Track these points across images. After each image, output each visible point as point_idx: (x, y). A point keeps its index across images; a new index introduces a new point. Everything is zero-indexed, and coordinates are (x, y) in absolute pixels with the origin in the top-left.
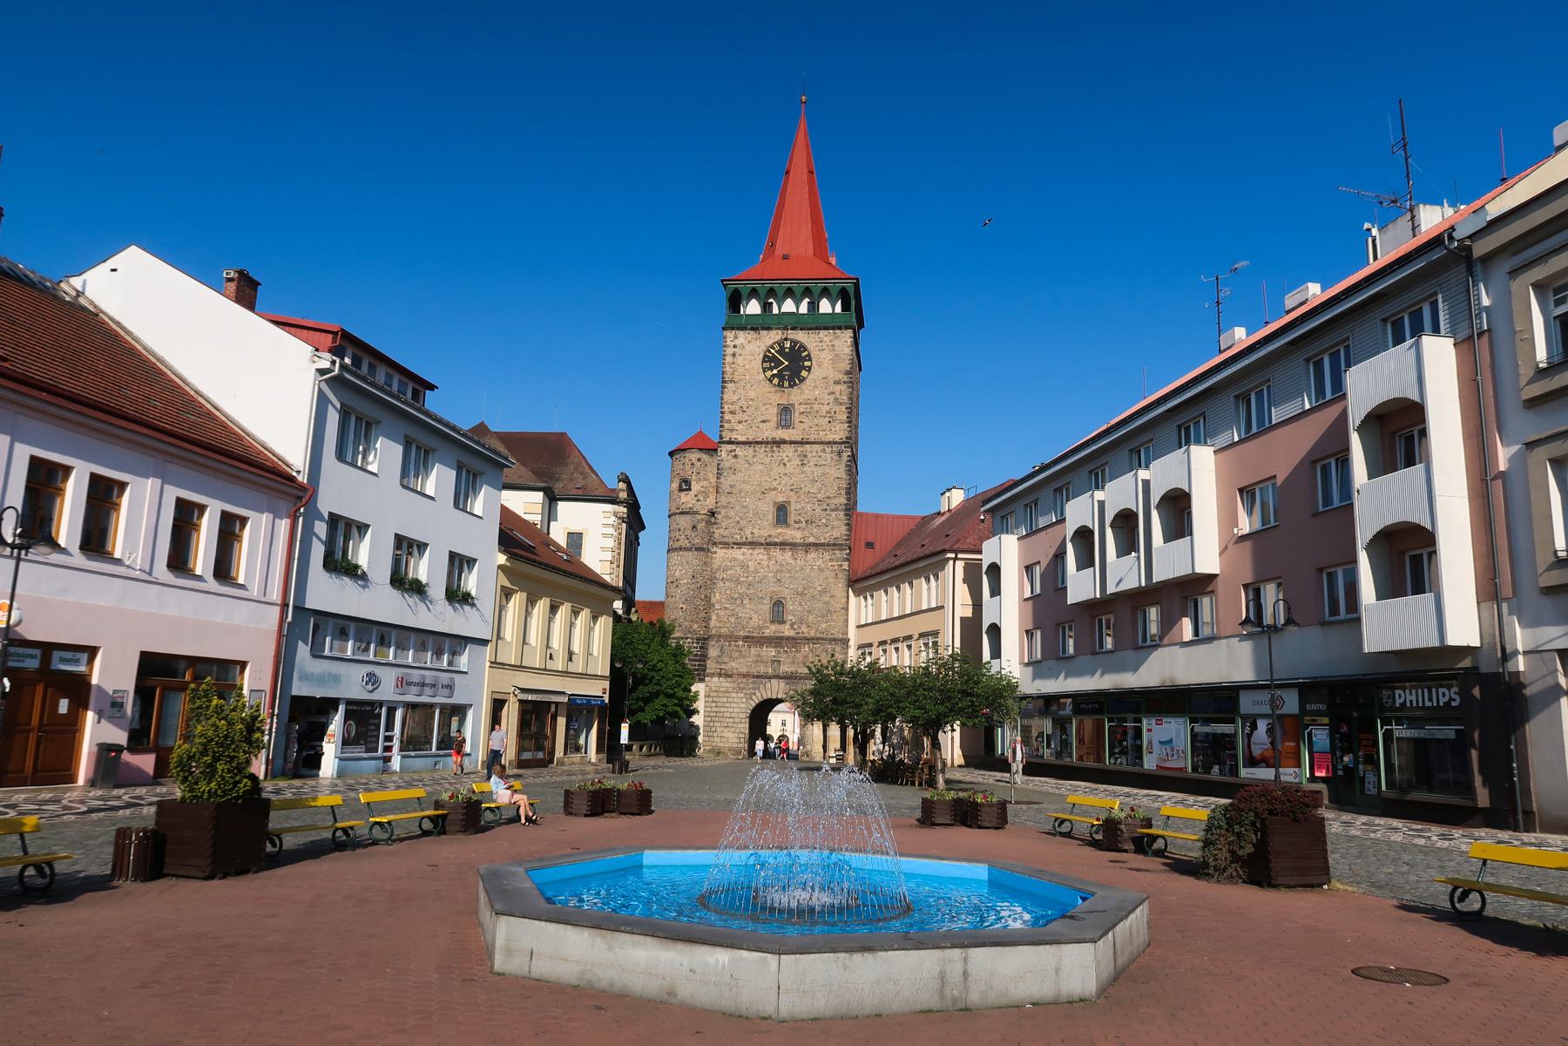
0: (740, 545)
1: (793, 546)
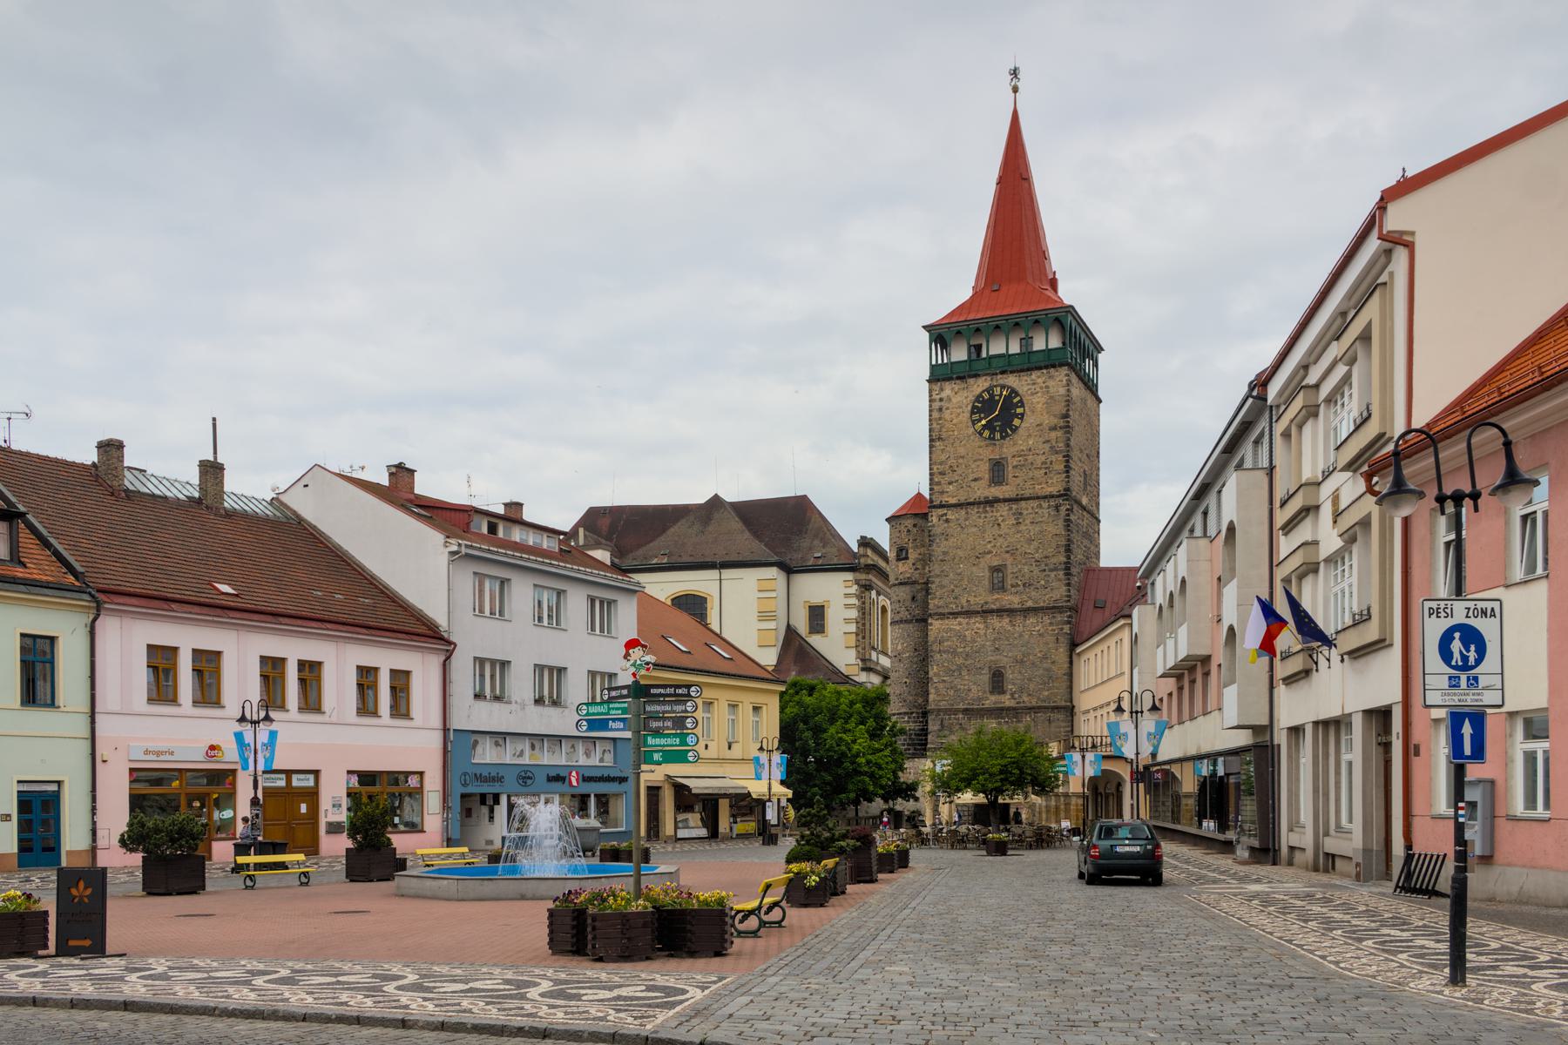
0: (955, 615)
1: (1011, 612)
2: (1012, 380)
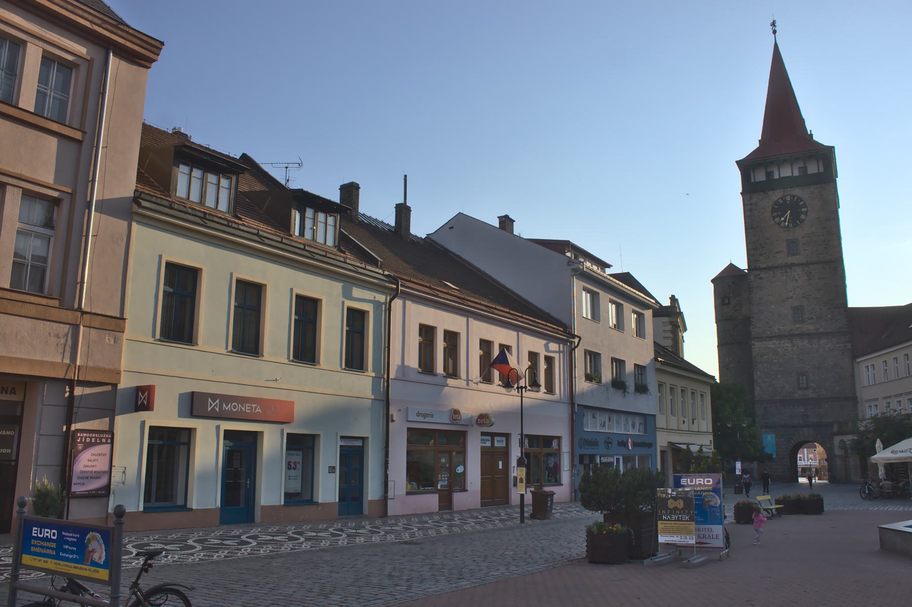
0: (771, 338)
1: (809, 335)
2: (797, 192)
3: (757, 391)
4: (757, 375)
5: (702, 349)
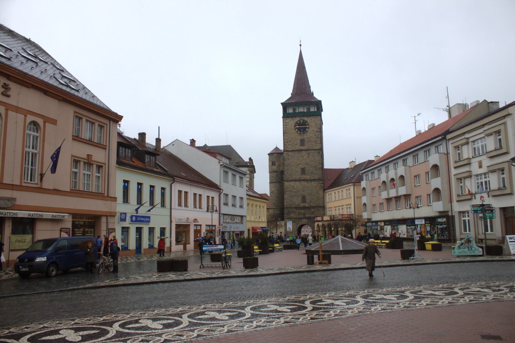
0: (292, 181)
1: (307, 180)
2: (305, 119)
3: (285, 204)
4: (285, 196)
5: (262, 183)
